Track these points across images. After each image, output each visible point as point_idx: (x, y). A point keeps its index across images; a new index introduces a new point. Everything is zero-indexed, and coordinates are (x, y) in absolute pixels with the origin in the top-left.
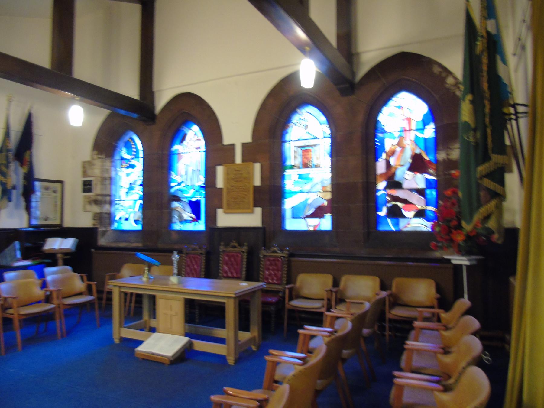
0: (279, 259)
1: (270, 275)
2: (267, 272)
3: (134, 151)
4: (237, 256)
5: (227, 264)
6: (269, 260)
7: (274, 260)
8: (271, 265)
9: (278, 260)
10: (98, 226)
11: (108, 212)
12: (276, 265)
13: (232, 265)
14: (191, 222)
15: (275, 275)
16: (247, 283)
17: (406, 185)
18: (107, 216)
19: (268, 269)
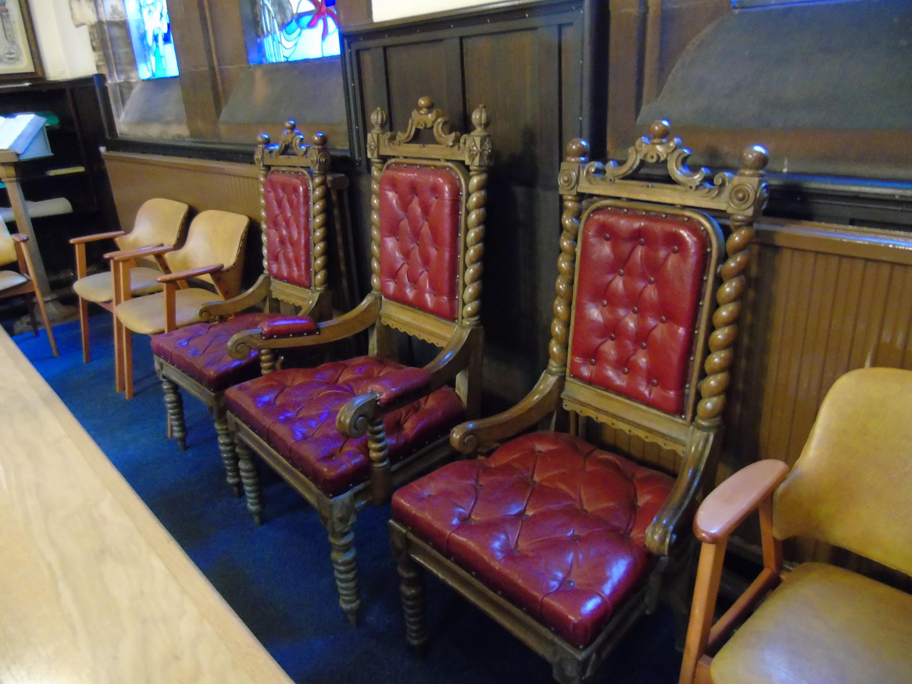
0: (684, 233)
1: (612, 330)
2: (595, 313)
3: (379, 432)
4: (436, 190)
5: (393, 229)
6: (605, 231)
7: (637, 236)
8: (620, 264)
9: (675, 241)
10: (104, 71)
11: (117, 18)
12: (654, 269)
13: (417, 235)
14: (716, 271)
15: (643, 337)
16: (535, 401)
17: (139, 17)
18: (116, 32)
19: (602, 294)
